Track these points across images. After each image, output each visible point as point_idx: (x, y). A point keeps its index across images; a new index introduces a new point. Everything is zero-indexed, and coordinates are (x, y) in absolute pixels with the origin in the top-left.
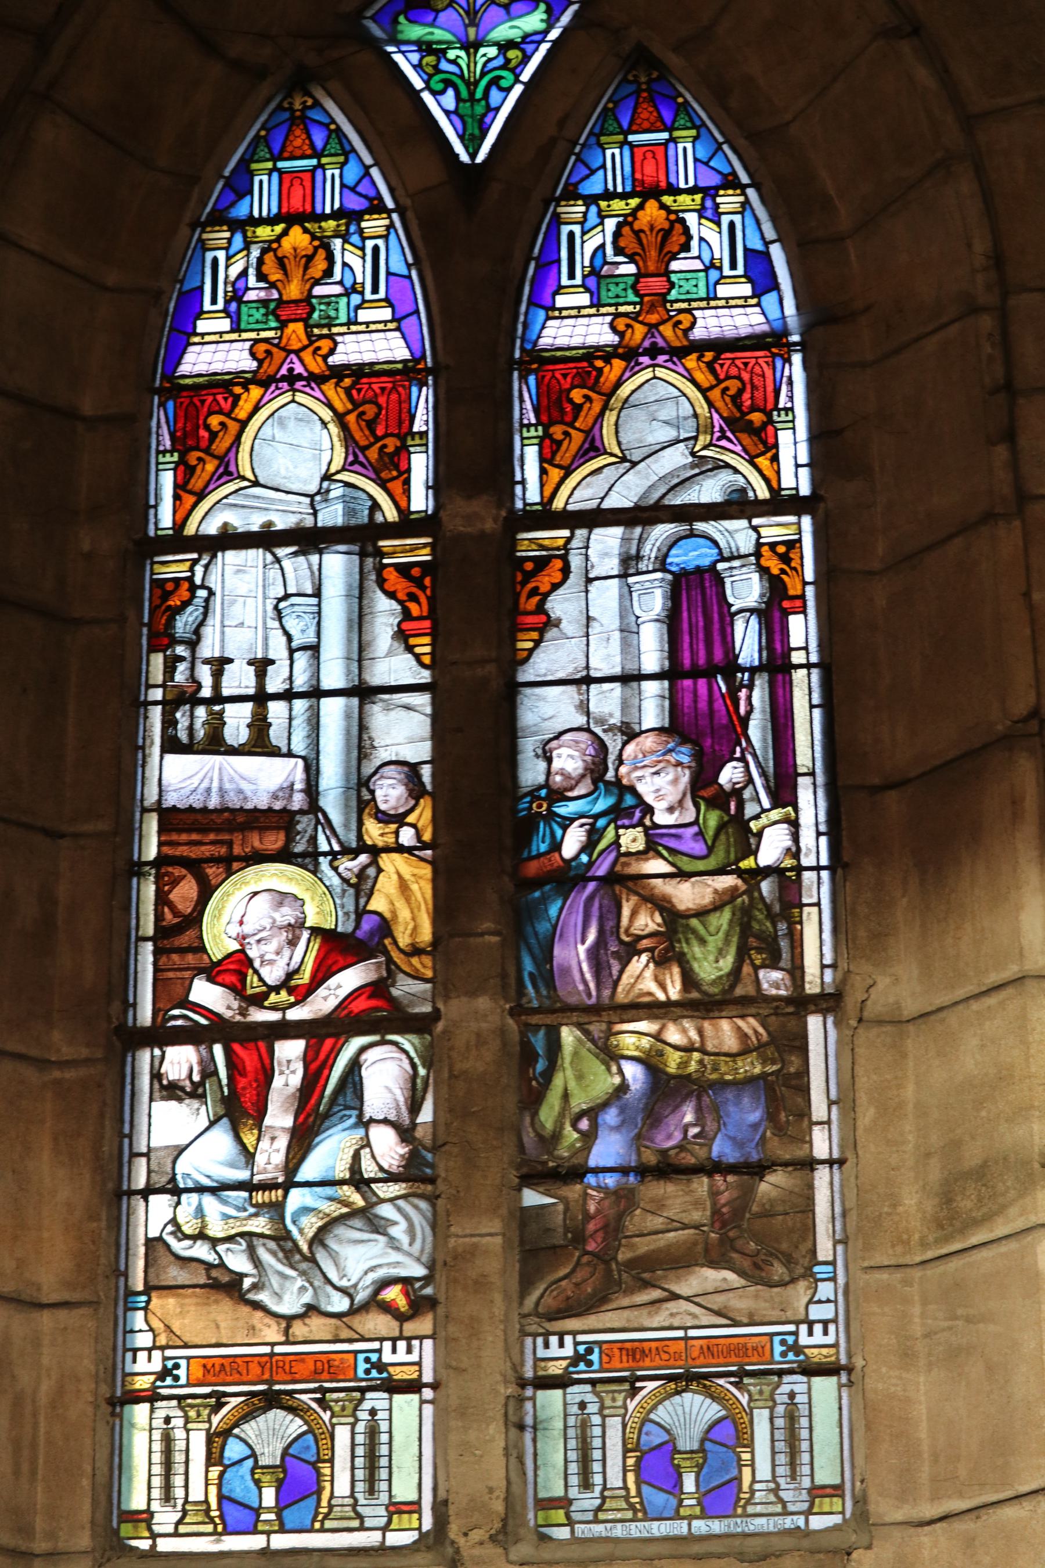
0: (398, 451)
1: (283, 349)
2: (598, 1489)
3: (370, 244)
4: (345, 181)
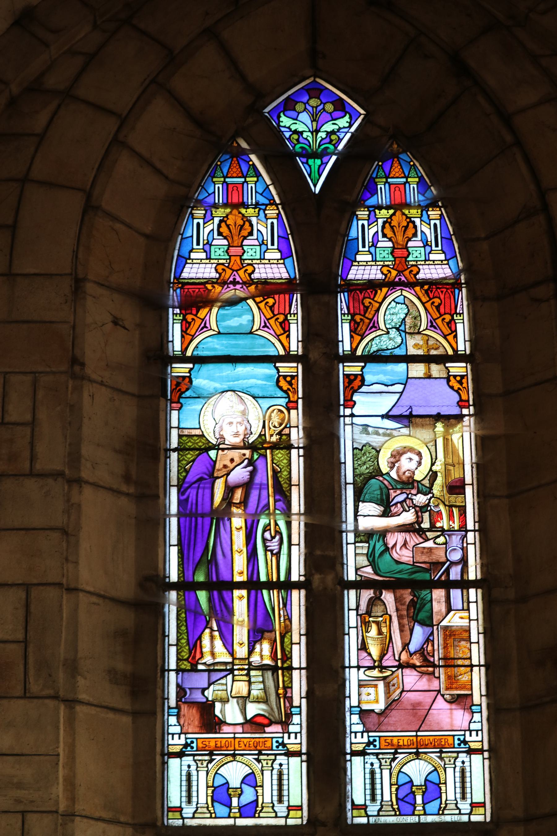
0: (284, 321)
1: (231, 269)
2: (379, 802)
3: (269, 221)
4: (258, 190)
